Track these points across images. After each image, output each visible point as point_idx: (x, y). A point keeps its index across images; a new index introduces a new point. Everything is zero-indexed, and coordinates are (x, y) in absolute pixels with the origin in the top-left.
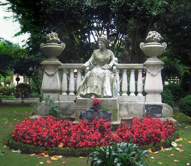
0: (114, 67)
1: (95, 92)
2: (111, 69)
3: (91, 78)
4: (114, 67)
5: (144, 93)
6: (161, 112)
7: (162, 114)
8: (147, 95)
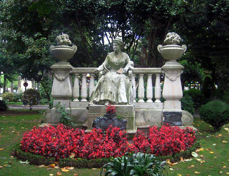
0: (129, 71)
1: (110, 99)
2: (127, 74)
3: (105, 83)
4: (129, 71)
5: (163, 100)
6: (181, 120)
7: (181, 122)
8: (165, 102)
